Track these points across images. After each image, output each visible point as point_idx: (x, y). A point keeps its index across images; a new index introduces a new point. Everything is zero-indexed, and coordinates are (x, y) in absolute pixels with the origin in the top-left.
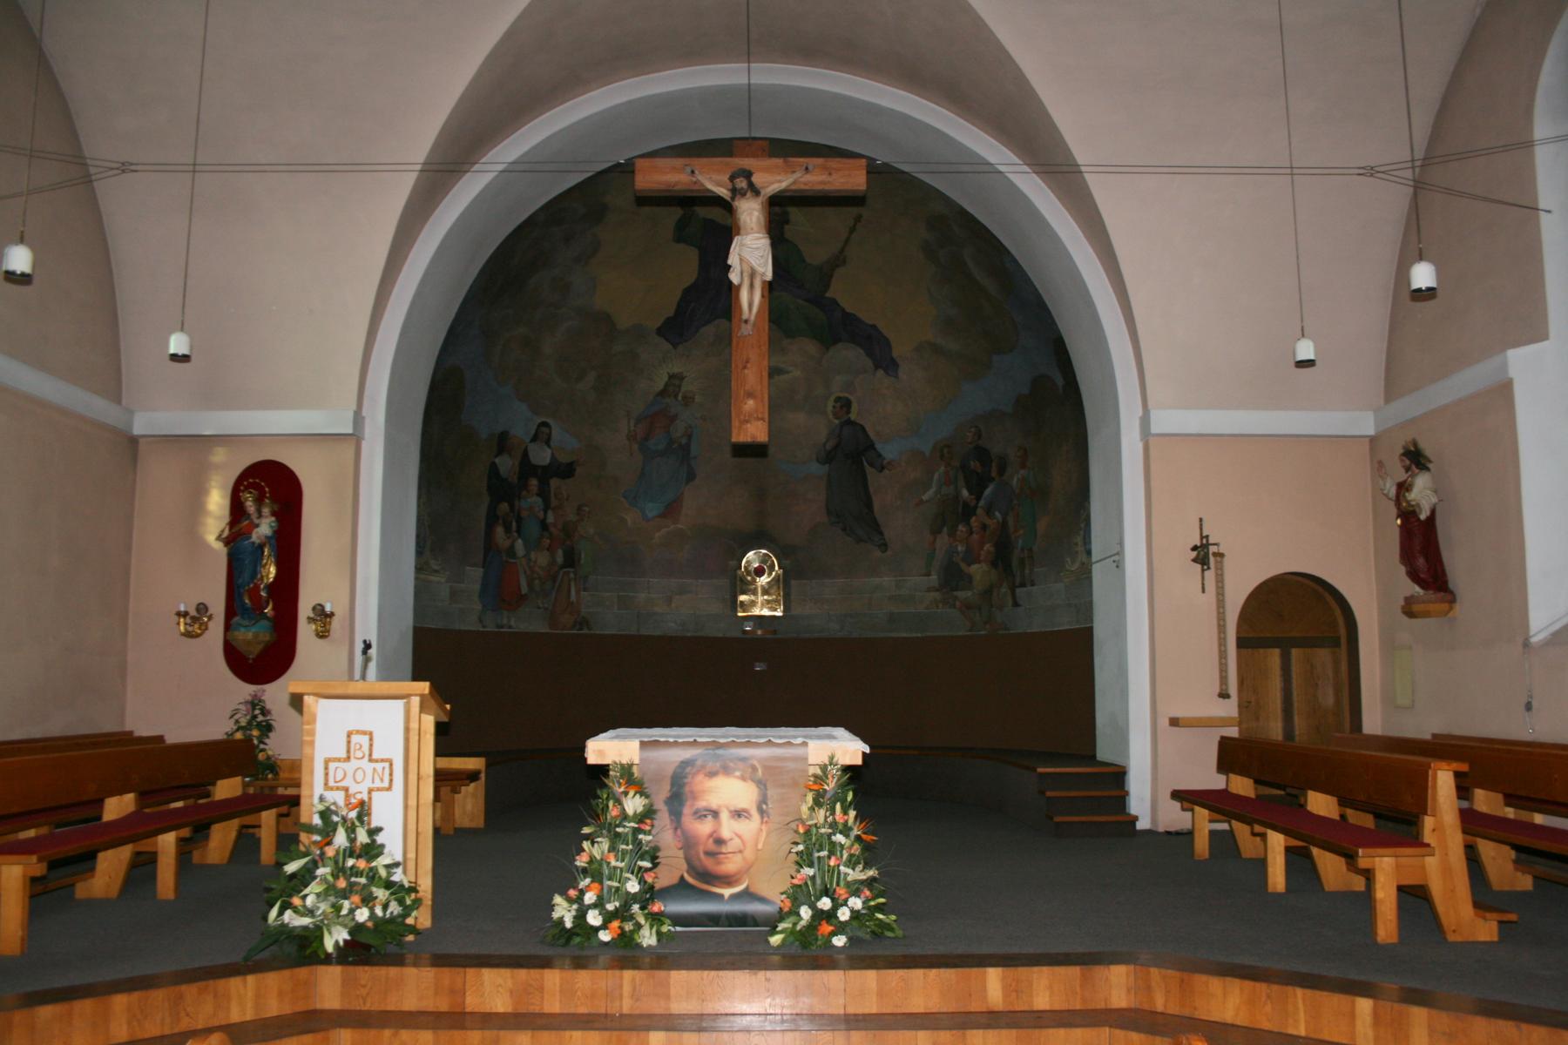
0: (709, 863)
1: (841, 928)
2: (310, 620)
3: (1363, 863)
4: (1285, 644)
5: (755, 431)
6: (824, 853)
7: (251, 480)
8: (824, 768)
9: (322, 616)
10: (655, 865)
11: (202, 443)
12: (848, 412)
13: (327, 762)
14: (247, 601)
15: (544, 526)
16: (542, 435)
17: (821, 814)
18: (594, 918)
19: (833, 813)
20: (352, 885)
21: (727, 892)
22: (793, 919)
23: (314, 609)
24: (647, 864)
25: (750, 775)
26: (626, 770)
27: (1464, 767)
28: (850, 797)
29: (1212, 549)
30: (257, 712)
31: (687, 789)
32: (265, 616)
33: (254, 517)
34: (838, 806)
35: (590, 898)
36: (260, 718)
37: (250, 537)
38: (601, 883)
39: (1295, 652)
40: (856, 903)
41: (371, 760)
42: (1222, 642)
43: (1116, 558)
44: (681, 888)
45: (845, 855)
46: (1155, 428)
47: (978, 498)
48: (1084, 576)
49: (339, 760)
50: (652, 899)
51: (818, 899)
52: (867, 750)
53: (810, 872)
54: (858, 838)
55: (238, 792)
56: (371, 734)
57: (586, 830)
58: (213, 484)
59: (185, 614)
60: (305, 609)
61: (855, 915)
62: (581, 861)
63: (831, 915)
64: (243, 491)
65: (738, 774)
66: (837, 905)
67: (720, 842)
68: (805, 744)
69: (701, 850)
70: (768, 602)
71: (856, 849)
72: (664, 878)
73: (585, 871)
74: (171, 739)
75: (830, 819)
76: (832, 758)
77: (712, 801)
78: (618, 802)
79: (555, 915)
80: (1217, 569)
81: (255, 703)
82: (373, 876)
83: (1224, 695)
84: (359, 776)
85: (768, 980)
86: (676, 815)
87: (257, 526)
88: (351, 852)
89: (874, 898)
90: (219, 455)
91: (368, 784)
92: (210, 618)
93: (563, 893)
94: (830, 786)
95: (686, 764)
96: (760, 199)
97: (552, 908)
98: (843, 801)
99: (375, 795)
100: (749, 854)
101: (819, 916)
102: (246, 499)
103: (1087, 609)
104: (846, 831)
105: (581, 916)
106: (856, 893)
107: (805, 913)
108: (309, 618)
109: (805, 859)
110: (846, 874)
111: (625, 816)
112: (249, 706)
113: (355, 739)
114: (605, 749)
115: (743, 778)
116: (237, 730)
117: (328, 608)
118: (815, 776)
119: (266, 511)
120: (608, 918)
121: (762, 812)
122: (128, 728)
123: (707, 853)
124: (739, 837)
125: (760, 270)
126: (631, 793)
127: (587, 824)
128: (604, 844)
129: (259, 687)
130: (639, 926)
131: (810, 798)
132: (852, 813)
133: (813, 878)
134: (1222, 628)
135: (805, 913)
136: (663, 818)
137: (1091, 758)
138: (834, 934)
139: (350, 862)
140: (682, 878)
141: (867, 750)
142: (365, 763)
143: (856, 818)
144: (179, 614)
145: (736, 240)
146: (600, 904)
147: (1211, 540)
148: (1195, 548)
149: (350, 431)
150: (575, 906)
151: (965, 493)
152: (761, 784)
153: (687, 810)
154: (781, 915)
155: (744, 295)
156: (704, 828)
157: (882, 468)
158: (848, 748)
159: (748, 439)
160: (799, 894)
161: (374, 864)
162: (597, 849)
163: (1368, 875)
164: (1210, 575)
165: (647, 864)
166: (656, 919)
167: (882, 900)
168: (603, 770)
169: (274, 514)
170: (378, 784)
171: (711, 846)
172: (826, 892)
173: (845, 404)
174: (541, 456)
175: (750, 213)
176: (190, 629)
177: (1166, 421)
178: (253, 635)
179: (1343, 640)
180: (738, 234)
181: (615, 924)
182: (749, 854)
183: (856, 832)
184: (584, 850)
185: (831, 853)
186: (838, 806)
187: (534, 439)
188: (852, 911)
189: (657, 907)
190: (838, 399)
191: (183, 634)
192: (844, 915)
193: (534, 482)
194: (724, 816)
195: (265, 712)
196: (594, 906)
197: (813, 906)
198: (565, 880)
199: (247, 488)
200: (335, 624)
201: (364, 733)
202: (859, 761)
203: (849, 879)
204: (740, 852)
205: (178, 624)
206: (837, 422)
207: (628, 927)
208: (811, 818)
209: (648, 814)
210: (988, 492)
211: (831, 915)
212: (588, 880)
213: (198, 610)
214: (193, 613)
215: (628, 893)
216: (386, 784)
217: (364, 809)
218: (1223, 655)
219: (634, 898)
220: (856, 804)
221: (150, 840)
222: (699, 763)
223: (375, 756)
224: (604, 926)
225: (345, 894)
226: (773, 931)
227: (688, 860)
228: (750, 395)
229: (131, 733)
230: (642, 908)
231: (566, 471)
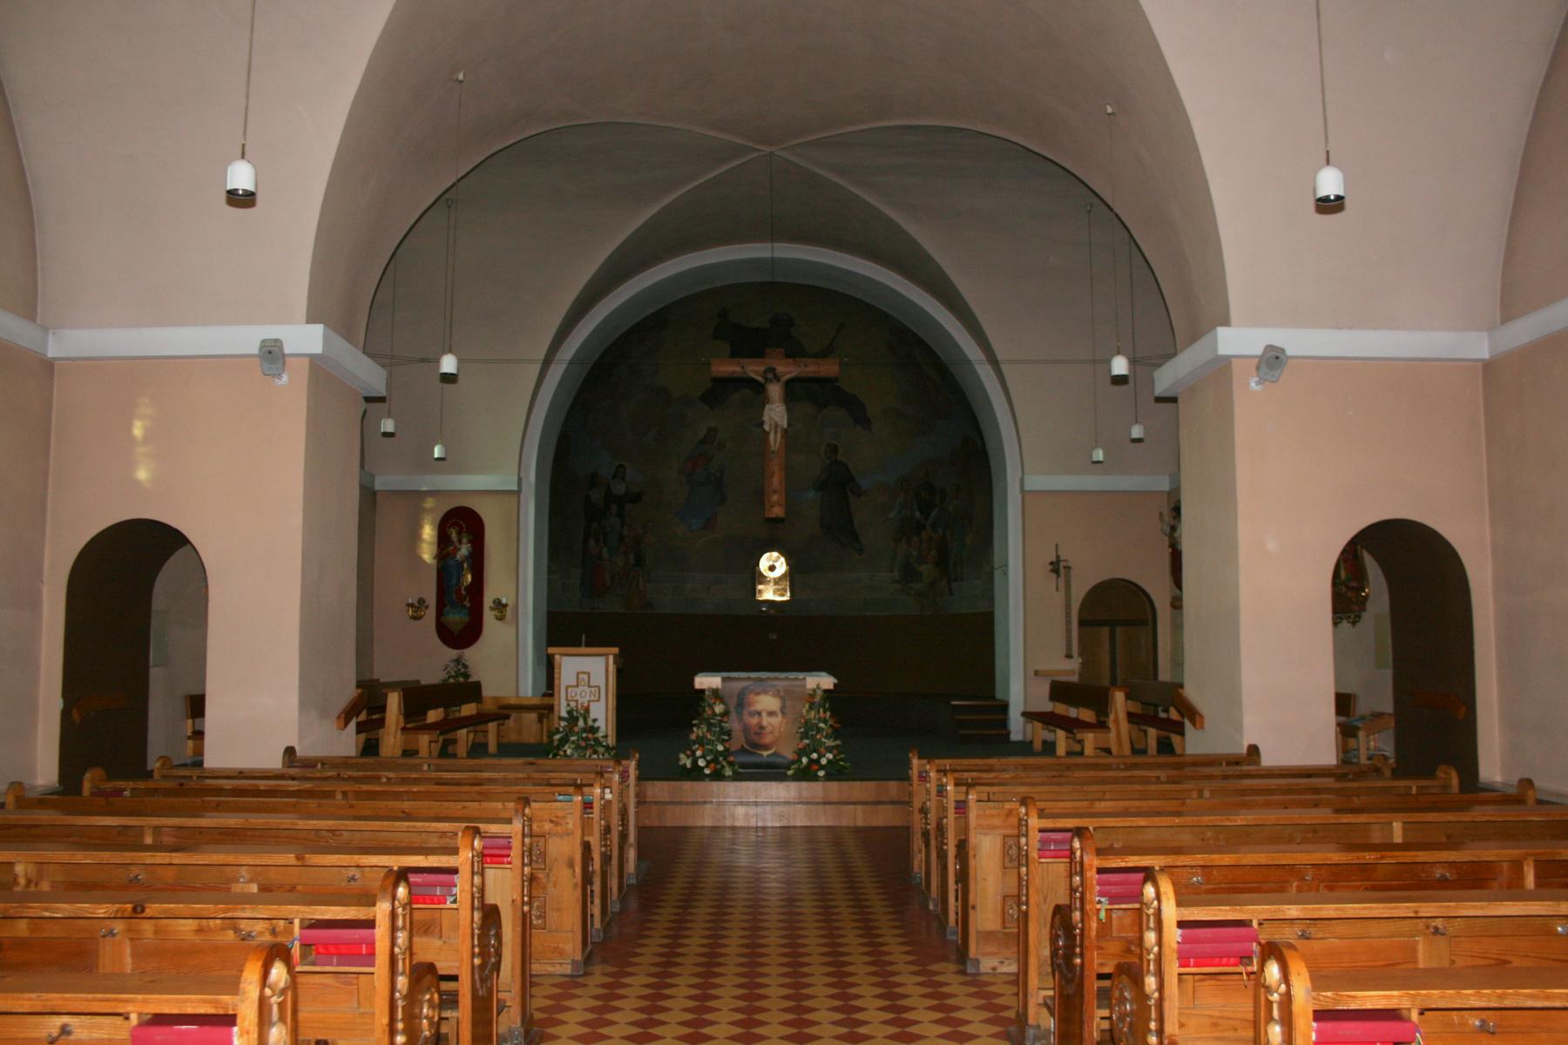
0: (755, 738)
1: (823, 767)
2: (492, 609)
3: (1079, 736)
4: (1112, 624)
5: (777, 512)
6: (814, 733)
7: (454, 520)
8: (814, 690)
9: (499, 606)
10: (730, 738)
11: (420, 495)
12: (836, 454)
13: (567, 687)
14: (454, 596)
15: (622, 538)
16: (619, 474)
17: (813, 713)
18: (701, 763)
19: (819, 712)
20: (587, 745)
21: (765, 753)
22: (799, 763)
23: (494, 602)
24: (726, 738)
25: (777, 694)
26: (715, 692)
27: (1127, 690)
28: (827, 706)
29: (1062, 564)
30: (460, 667)
31: (745, 701)
32: (464, 607)
33: (457, 544)
34: (821, 710)
35: (699, 753)
36: (463, 670)
37: (456, 557)
38: (703, 747)
39: (1118, 629)
40: (830, 756)
41: (577, 686)
42: (1068, 622)
43: (1004, 568)
44: (743, 751)
45: (825, 734)
46: (1027, 488)
47: (927, 519)
48: (991, 578)
49: (572, 686)
50: (729, 755)
51: (811, 753)
52: (836, 681)
53: (807, 741)
54: (831, 726)
55: (474, 712)
56: (589, 674)
57: (695, 722)
58: (426, 521)
59: (411, 605)
60: (488, 601)
61: (829, 761)
62: (693, 737)
63: (817, 761)
64: (449, 527)
65: (771, 693)
66: (820, 756)
67: (762, 728)
68: (804, 679)
69: (752, 731)
70: (778, 590)
71: (830, 731)
72: (734, 746)
73: (695, 742)
74: (423, 682)
75: (817, 717)
76: (818, 685)
77: (758, 707)
78: (711, 707)
79: (681, 763)
80: (1065, 576)
81: (458, 661)
82: (596, 740)
83: (1069, 656)
84: (583, 694)
85: (787, 786)
86: (740, 714)
87: (459, 550)
88: (584, 730)
89: (838, 755)
90: (429, 503)
91: (588, 698)
92: (427, 607)
93: (684, 753)
94: (817, 699)
95: (745, 689)
96: (781, 383)
97: (679, 760)
98: (824, 707)
99: (591, 704)
100: (776, 734)
101: (811, 761)
102: (451, 533)
103: (991, 601)
104: (825, 722)
105: (695, 762)
106: (830, 752)
107: (805, 760)
108: (491, 607)
109: (805, 736)
110: (825, 743)
111: (714, 714)
112: (456, 663)
113: (581, 676)
114: (706, 681)
115: (774, 696)
116: (449, 677)
117: (504, 601)
118: (810, 695)
119: (465, 540)
120: (708, 763)
121: (783, 713)
122: (375, 677)
123: (755, 733)
124: (772, 725)
125: (780, 423)
126: (718, 703)
127: (695, 719)
128: (704, 728)
129: (461, 651)
130: (723, 767)
131: (807, 706)
132: (828, 714)
133: (808, 745)
134: (1068, 615)
135: (805, 760)
136: (733, 715)
137: (993, 697)
138: (819, 770)
139: (584, 735)
140: (742, 746)
141: (836, 681)
142: (586, 688)
143: (830, 716)
144: (408, 605)
145: (767, 407)
146: (703, 757)
147: (1062, 558)
148: (1052, 563)
149: (516, 488)
150: (691, 758)
151: (918, 514)
152: (782, 698)
153: (745, 712)
154: (793, 762)
155: (772, 436)
156: (754, 721)
157: (859, 495)
158: (826, 681)
159: (774, 516)
160: (801, 752)
161: (596, 736)
162: (698, 732)
163: (1080, 742)
164: (1062, 579)
165: (726, 738)
166: (731, 764)
167: (843, 756)
168: (702, 691)
169: (469, 542)
170: (593, 698)
171: (757, 729)
172: (815, 751)
173: (834, 449)
174: (619, 488)
175: (775, 391)
176: (415, 614)
177: (1036, 482)
178: (456, 618)
179: (1150, 622)
180: (768, 402)
181: (712, 765)
182: (776, 733)
183: (830, 723)
184: (693, 731)
185: (818, 732)
186: (821, 710)
187: (615, 476)
188: (827, 759)
189: (731, 759)
190: (828, 445)
191: (411, 618)
192: (824, 761)
193: (614, 507)
194: (764, 715)
195: (465, 666)
196: (701, 757)
197: (808, 757)
198: (687, 747)
199: (451, 525)
200: (509, 612)
201: (585, 673)
202: (831, 687)
203: (827, 745)
204: (772, 733)
205: (408, 611)
206: (828, 461)
207: (719, 766)
208: (808, 715)
209: (726, 713)
210: (933, 514)
211: (817, 761)
212: (697, 746)
213: (419, 602)
214: (417, 604)
215: (717, 751)
216: (597, 698)
217: (587, 710)
218: (1069, 631)
219: (721, 753)
220: (831, 709)
221: (453, 734)
222: (752, 688)
223: (592, 684)
224: (707, 766)
225: (585, 748)
226: (789, 769)
227: (746, 738)
228: (775, 492)
229: (378, 680)
230: (724, 759)
231: (636, 498)
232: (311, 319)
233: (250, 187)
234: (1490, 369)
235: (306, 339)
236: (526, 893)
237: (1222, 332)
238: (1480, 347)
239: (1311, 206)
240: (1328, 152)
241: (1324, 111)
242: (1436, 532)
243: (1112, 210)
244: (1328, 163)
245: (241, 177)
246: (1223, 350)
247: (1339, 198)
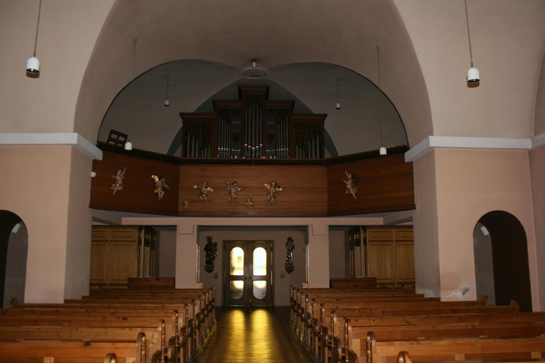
79: (121, 188)
232: (75, 131)
233: (37, 68)
234: (531, 153)
235: (72, 138)
236: (166, 291)
237: (431, 138)
238: (528, 144)
239: (466, 84)
240: (472, 62)
241: (470, 42)
242: (514, 216)
243: (379, 89)
244: (472, 66)
245: (33, 64)
246: (432, 145)
247: (477, 80)
